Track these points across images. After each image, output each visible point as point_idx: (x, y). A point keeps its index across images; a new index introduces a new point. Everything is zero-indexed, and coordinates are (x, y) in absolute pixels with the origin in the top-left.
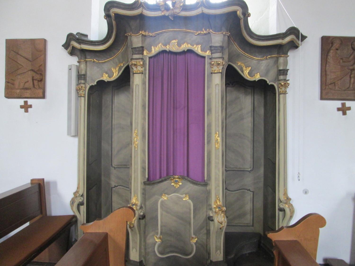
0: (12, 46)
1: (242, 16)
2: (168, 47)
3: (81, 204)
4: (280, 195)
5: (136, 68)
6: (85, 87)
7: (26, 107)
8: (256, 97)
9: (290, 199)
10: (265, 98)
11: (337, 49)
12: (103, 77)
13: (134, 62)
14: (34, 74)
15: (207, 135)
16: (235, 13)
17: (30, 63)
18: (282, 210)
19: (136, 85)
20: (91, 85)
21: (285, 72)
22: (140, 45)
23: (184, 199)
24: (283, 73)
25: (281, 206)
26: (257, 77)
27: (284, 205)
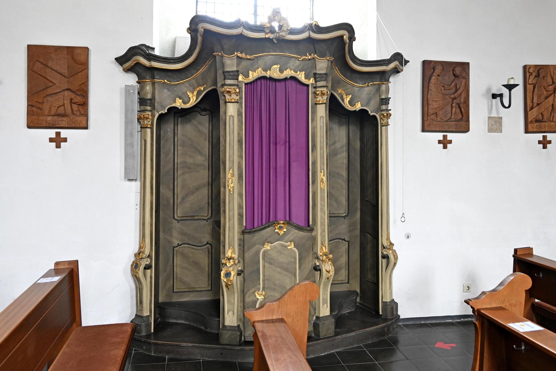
0: (38, 56)
1: (348, 41)
2: (268, 72)
3: (148, 267)
4: (383, 241)
5: (230, 96)
6: (153, 116)
7: (58, 141)
8: (351, 127)
9: (393, 245)
10: (362, 130)
11: (439, 76)
12: (175, 102)
13: (227, 88)
14: (73, 96)
15: (312, 174)
16: (342, 37)
17: (66, 80)
18: (386, 257)
19: (229, 117)
20: (160, 113)
21: (386, 101)
22: (235, 69)
23: (289, 248)
24: (386, 102)
25: (385, 253)
26: (358, 107)
27: (388, 251)
